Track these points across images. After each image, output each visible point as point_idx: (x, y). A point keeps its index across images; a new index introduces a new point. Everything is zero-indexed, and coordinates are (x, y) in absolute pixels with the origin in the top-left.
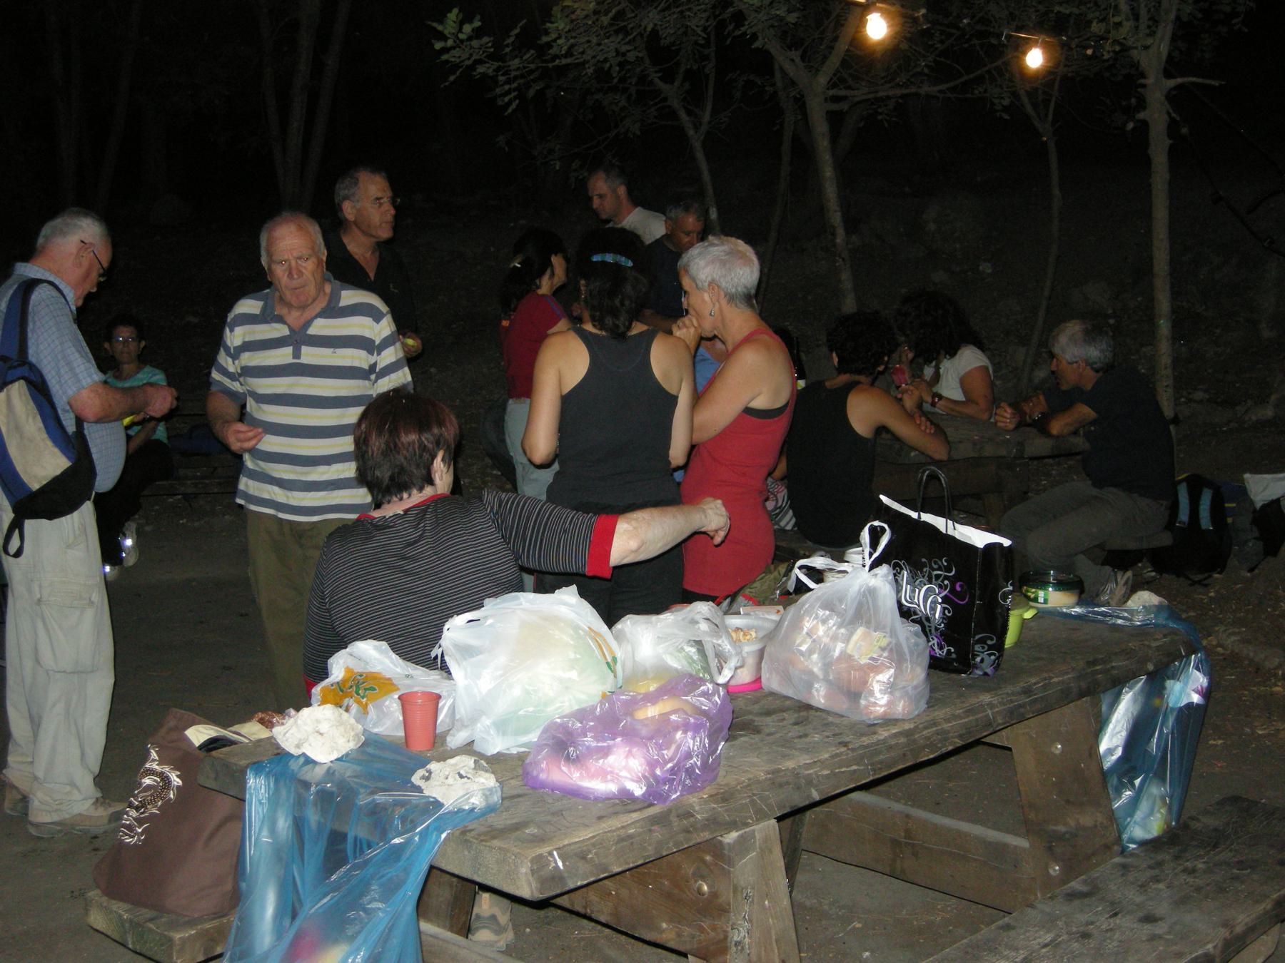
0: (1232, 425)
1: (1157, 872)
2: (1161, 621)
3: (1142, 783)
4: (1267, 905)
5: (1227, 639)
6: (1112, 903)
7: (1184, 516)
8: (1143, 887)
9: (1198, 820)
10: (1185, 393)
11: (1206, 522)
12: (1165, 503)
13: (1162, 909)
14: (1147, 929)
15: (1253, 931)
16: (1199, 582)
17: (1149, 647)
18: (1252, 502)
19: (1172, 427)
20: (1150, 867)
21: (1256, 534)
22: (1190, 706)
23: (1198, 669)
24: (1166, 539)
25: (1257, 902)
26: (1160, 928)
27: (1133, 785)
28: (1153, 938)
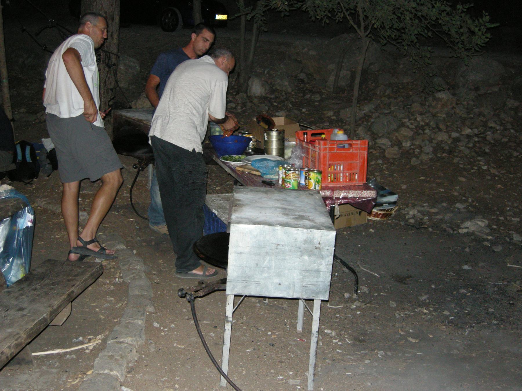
0: (36, 121)
1: (22, 292)
2: (12, 195)
3: (13, 260)
4: (65, 296)
5: (41, 203)
6: (6, 306)
7: (20, 157)
8: (17, 298)
9: (36, 270)
10: (17, 110)
11: (29, 159)
12: (11, 152)
13: (25, 305)
14: (20, 313)
15: (60, 307)
16: (28, 183)
17: (8, 206)
18: (46, 150)
19: (12, 123)
20: (19, 291)
21: (49, 162)
22: (27, 227)
23: (29, 213)
24: (13, 167)
25: (61, 296)
26: (25, 312)
27: (9, 262)
28: (23, 316)
